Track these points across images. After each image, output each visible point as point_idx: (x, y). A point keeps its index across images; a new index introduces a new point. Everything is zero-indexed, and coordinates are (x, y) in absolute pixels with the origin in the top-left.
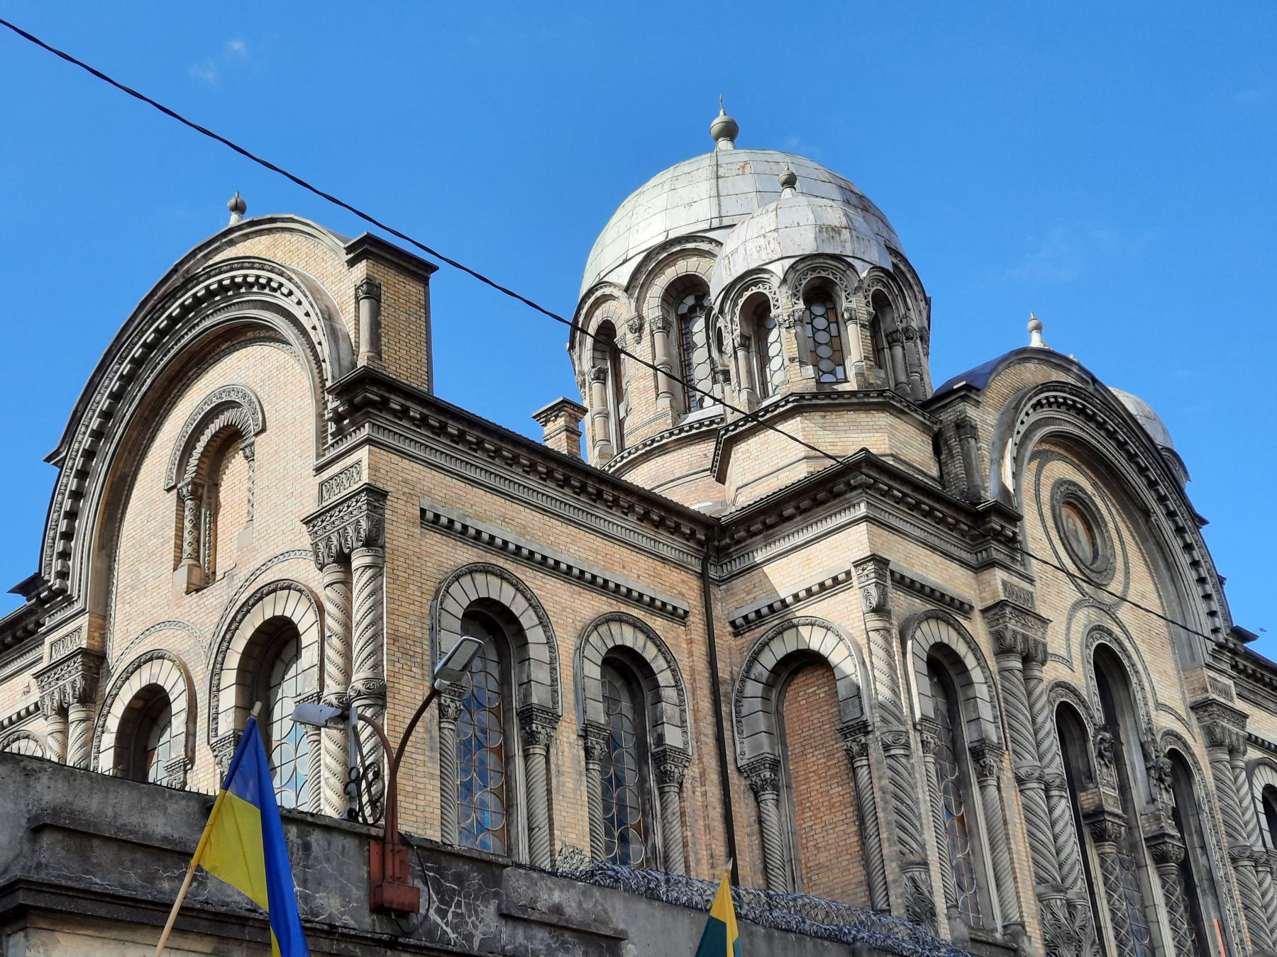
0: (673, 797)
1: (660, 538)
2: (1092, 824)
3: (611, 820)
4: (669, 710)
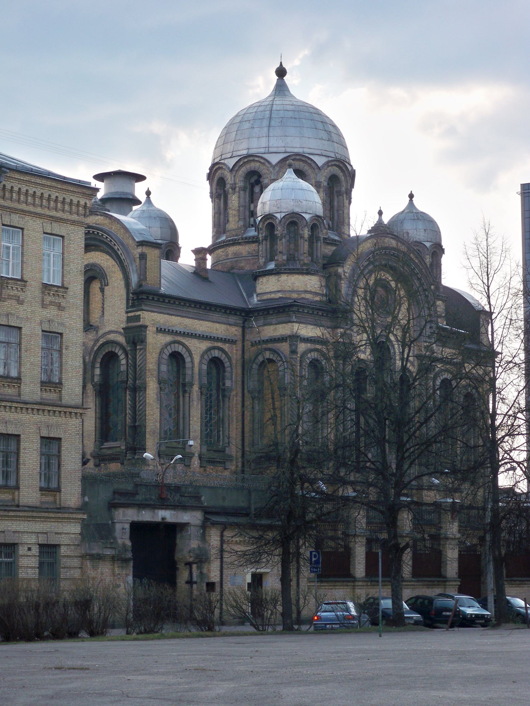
1: (230, 317)
3: (207, 410)
4: (227, 374)
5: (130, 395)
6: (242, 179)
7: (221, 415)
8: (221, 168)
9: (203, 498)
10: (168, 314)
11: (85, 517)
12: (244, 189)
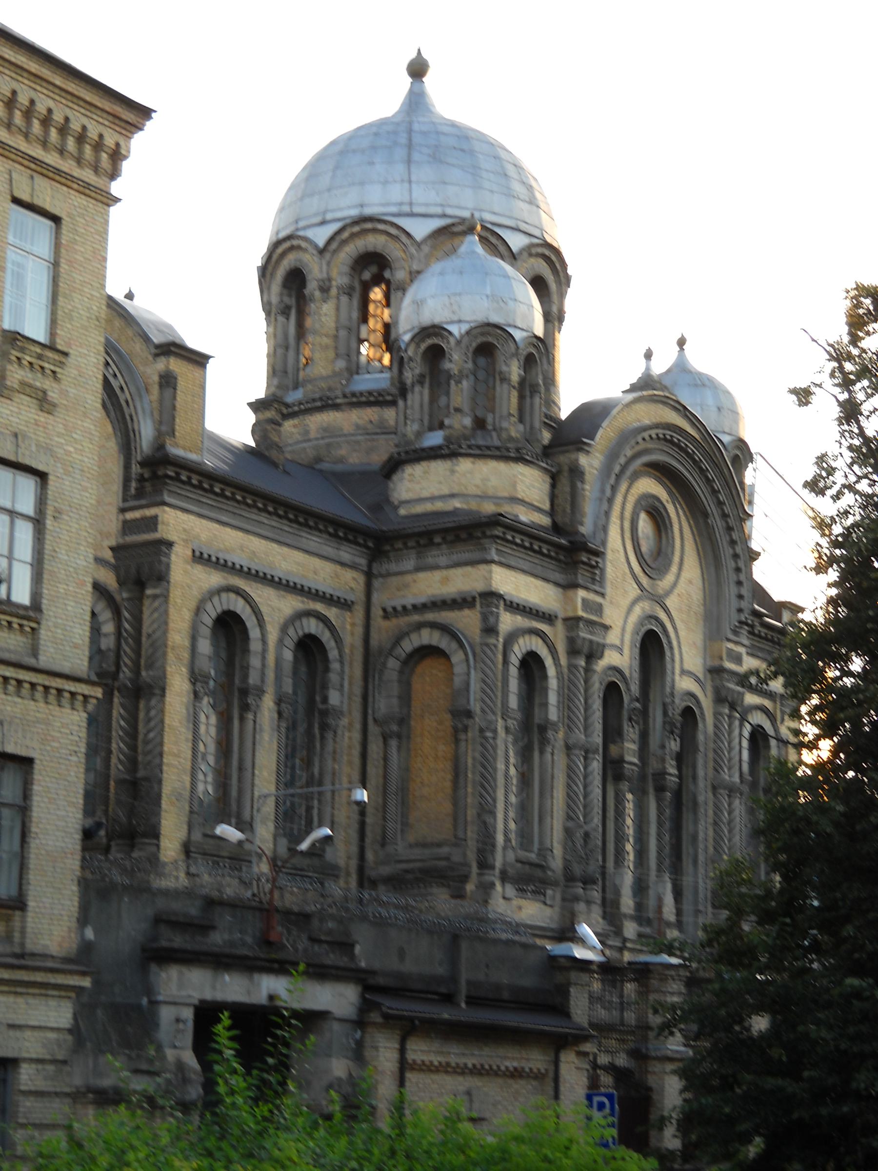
0: (330, 741)
1: (343, 548)
2: (613, 769)
4: (333, 677)
5: (122, 705)
6: (346, 269)
7: (316, 771)
8: (299, 248)
9: (358, 949)
10: (218, 522)
11: (86, 982)
12: (349, 291)
